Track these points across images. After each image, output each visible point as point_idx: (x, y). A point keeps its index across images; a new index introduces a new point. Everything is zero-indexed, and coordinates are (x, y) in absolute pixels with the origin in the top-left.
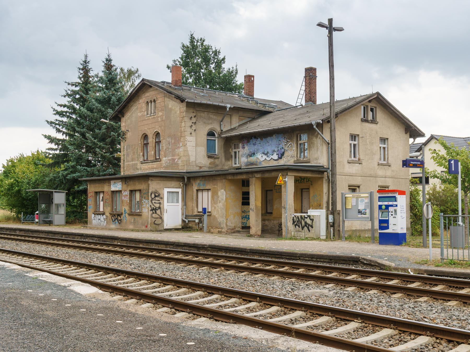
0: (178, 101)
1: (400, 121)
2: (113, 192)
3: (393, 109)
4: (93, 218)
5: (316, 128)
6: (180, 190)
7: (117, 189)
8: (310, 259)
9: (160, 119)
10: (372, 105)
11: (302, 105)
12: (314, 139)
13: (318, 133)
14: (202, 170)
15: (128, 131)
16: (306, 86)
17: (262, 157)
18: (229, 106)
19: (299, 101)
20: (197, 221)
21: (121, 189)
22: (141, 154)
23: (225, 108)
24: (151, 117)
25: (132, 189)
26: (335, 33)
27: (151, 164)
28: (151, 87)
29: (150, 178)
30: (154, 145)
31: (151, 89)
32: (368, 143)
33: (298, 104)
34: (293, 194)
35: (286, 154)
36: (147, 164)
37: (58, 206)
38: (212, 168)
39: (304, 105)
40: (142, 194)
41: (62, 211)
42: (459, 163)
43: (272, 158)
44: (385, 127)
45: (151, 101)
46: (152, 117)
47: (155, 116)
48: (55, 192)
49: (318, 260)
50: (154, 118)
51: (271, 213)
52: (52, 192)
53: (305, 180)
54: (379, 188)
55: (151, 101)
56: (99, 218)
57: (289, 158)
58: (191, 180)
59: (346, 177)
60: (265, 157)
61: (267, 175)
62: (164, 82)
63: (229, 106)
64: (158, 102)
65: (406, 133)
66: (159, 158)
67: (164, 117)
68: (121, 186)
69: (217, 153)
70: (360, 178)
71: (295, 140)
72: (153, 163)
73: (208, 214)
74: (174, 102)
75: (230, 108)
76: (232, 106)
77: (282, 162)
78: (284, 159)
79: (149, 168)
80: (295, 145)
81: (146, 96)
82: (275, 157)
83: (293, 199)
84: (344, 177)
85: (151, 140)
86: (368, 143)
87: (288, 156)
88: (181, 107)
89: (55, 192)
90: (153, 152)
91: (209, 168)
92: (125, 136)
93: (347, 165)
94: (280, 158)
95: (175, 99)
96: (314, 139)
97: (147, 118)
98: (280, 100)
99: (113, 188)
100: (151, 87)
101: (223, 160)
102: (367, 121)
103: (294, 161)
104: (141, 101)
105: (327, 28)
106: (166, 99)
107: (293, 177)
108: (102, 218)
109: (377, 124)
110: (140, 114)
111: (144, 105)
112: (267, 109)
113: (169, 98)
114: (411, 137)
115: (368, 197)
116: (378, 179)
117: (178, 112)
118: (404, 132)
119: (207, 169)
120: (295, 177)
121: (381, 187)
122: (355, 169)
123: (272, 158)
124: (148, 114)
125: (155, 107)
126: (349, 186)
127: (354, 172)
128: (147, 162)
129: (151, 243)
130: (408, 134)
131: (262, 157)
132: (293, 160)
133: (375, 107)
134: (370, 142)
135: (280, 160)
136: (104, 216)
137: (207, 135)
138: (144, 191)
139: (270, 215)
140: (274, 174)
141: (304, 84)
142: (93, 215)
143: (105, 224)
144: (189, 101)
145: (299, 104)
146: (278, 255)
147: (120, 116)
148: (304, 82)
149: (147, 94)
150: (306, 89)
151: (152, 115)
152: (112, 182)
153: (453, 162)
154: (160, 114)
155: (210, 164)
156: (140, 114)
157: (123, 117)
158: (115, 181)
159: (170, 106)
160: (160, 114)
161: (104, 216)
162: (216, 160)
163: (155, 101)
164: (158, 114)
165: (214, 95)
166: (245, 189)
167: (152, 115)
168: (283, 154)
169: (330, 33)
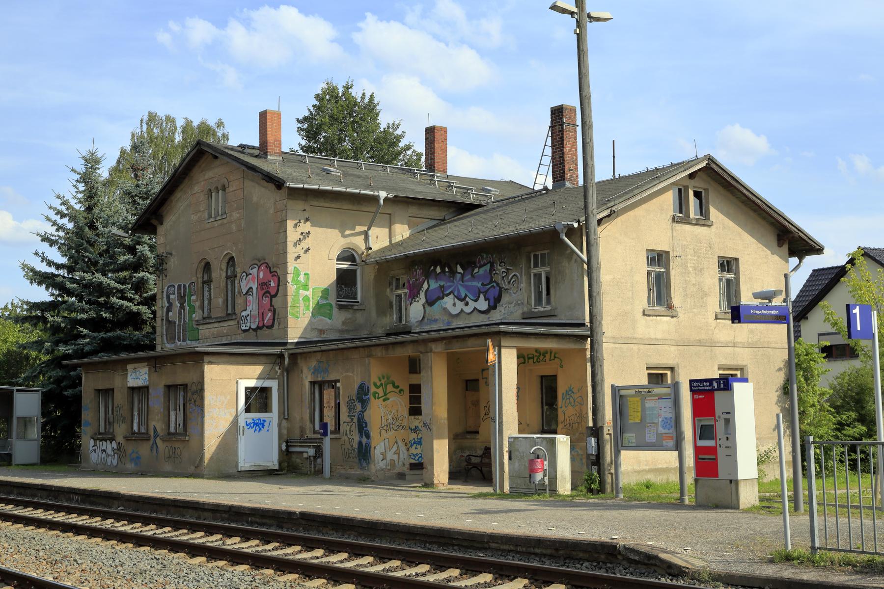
0: (271, 186)
1: (764, 218)
2: (133, 389)
3: (745, 191)
4: (91, 448)
5: (566, 239)
6: (273, 384)
7: (139, 383)
8: (512, 548)
9: (234, 227)
10: (697, 185)
11: (546, 188)
12: (565, 263)
13: (573, 251)
14: (324, 337)
15: (171, 254)
16: (553, 146)
17: (454, 305)
18: (383, 194)
19: (541, 179)
20: (311, 452)
21: (146, 384)
22: (197, 304)
23: (376, 199)
24: (216, 224)
25: (170, 382)
26: (591, 26)
27: (216, 325)
28: (216, 157)
29: (206, 359)
30: (223, 284)
31: (217, 162)
32: (691, 269)
33: (537, 188)
34: (515, 391)
35: (505, 298)
36: (209, 326)
37: (26, 422)
38: (348, 331)
39: (550, 187)
40: (189, 394)
41: (35, 432)
42: (874, 314)
43: (475, 308)
44: (726, 233)
45: (217, 188)
46: (219, 222)
47: (225, 221)
48: (18, 391)
49: (532, 550)
50: (222, 225)
51: (477, 432)
52: (12, 391)
53: (548, 356)
54: (721, 372)
55: (217, 188)
56: (104, 448)
57: (511, 306)
58: (299, 361)
59: (642, 347)
60: (460, 305)
61: (457, 348)
62: (243, 146)
63: (383, 194)
64: (231, 189)
65: (780, 245)
66: (234, 314)
67: (243, 223)
68: (147, 376)
69: (359, 299)
70: (673, 348)
71: (523, 266)
72: (222, 324)
73: (334, 436)
74: (263, 189)
75: (386, 199)
76: (391, 196)
77: (496, 316)
78: (502, 309)
79: (213, 334)
80: (524, 278)
81: (207, 177)
82: (483, 305)
83: (516, 402)
84: (635, 347)
85: (219, 273)
86: (691, 269)
87: (510, 303)
88: (278, 199)
89: (18, 391)
90: (220, 301)
91: (342, 331)
92: (165, 266)
93: (642, 321)
94: (493, 307)
95: (266, 184)
96: (565, 263)
97: (208, 226)
98: (508, 179)
99: (132, 382)
100: (216, 157)
101: (374, 313)
102: (686, 220)
103: (523, 313)
104: (197, 189)
105: (589, 16)
106: (248, 184)
107: (514, 352)
108: (109, 447)
109: (709, 226)
110: (194, 218)
111: (202, 197)
112: (472, 199)
113: (252, 181)
114: (792, 254)
115: (669, 395)
116: (717, 350)
117: (272, 211)
118: (775, 244)
119: (337, 336)
120: (519, 350)
121: (724, 369)
122: (661, 326)
123: (475, 308)
124: (210, 217)
125: (225, 201)
126: (648, 368)
127: (659, 336)
128: (208, 321)
129: (184, 507)
130: (785, 248)
131: (454, 305)
132: (520, 311)
133: (706, 190)
134: (695, 268)
135: (492, 312)
136: (114, 442)
137: (338, 260)
138: (194, 388)
139: (473, 436)
140: (472, 346)
141: (549, 142)
142: (92, 442)
143: (115, 462)
144: (292, 185)
145: (541, 187)
146: (435, 536)
147: (154, 222)
148: (549, 138)
149: (209, 174)
150: (553, 153)
151: (219, 218)
152: (130, 367)
153: (856, 311)
154: (236, 215)
155: (344, 323)
156: (194, 218)
157: (162, 224)
158: (136, 365)
159: (255, 199)
160: (236, 215)
161: (114, 444)
162: (359, 315)
163: (224, 189)
164: (231, 215)
165: (356, 172)
166: (414, 379)
167: (219, 218)
168: (498, 300)
169: (579, 24)
